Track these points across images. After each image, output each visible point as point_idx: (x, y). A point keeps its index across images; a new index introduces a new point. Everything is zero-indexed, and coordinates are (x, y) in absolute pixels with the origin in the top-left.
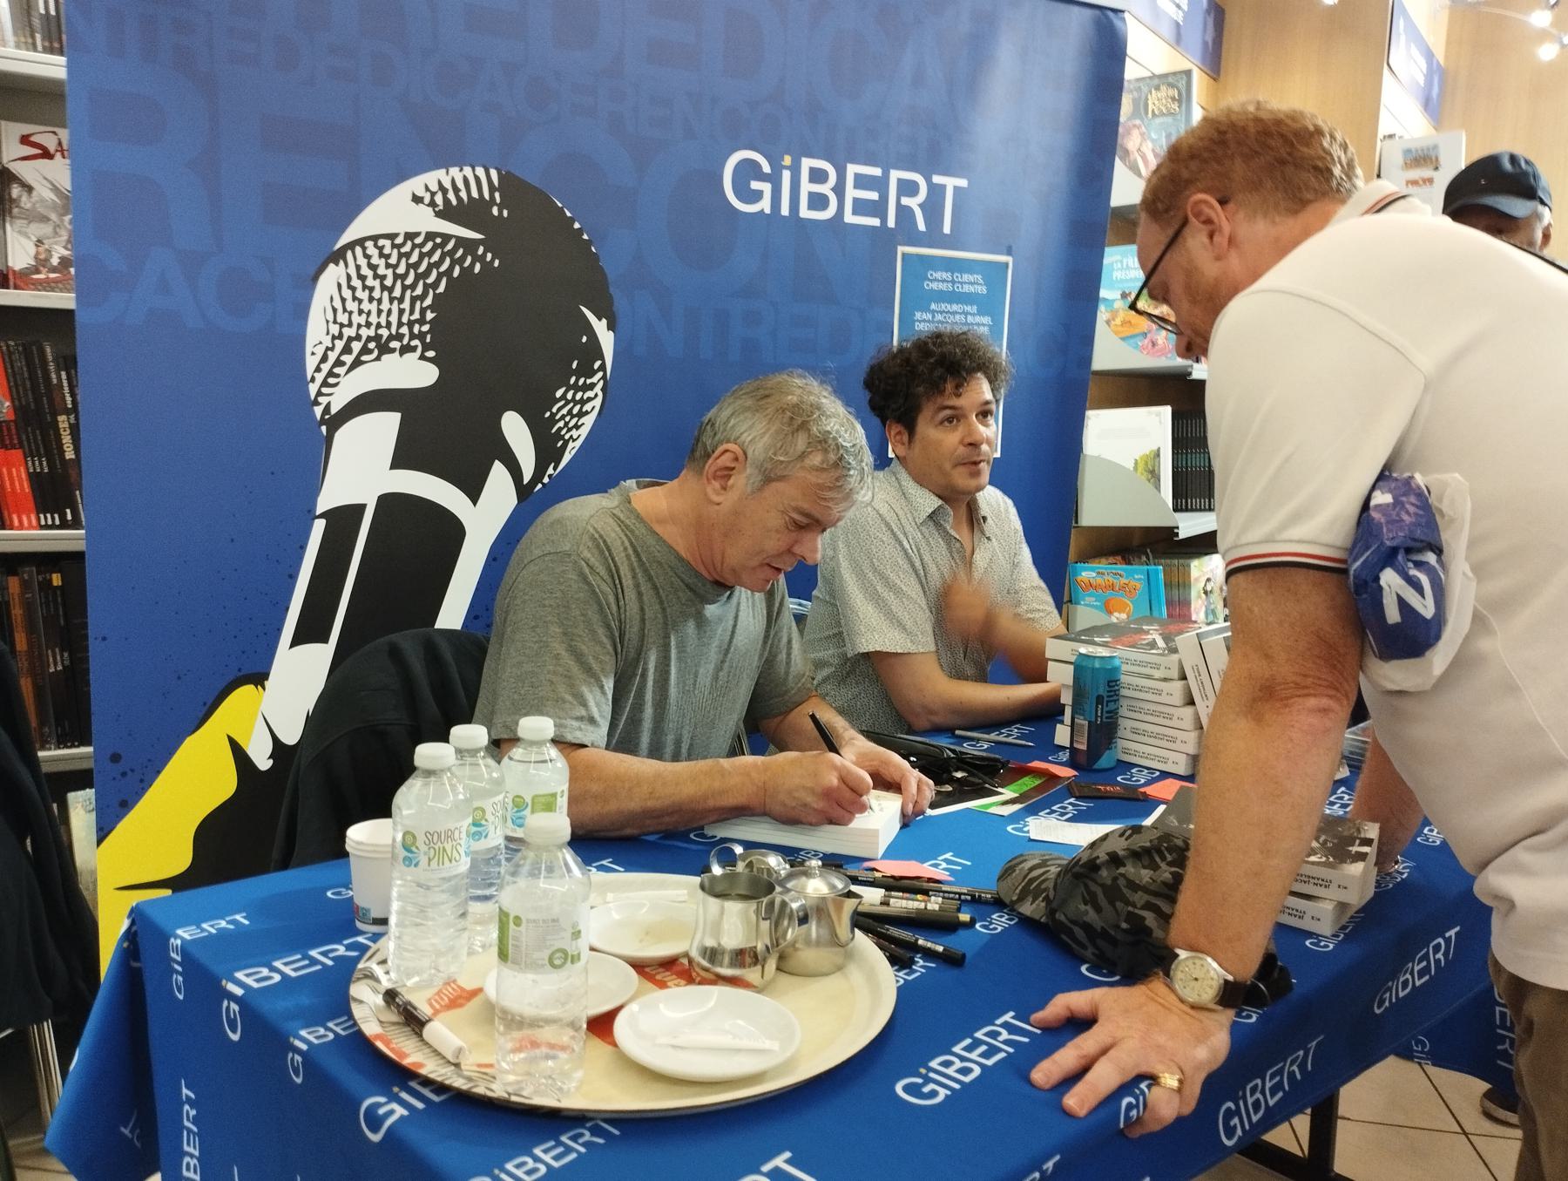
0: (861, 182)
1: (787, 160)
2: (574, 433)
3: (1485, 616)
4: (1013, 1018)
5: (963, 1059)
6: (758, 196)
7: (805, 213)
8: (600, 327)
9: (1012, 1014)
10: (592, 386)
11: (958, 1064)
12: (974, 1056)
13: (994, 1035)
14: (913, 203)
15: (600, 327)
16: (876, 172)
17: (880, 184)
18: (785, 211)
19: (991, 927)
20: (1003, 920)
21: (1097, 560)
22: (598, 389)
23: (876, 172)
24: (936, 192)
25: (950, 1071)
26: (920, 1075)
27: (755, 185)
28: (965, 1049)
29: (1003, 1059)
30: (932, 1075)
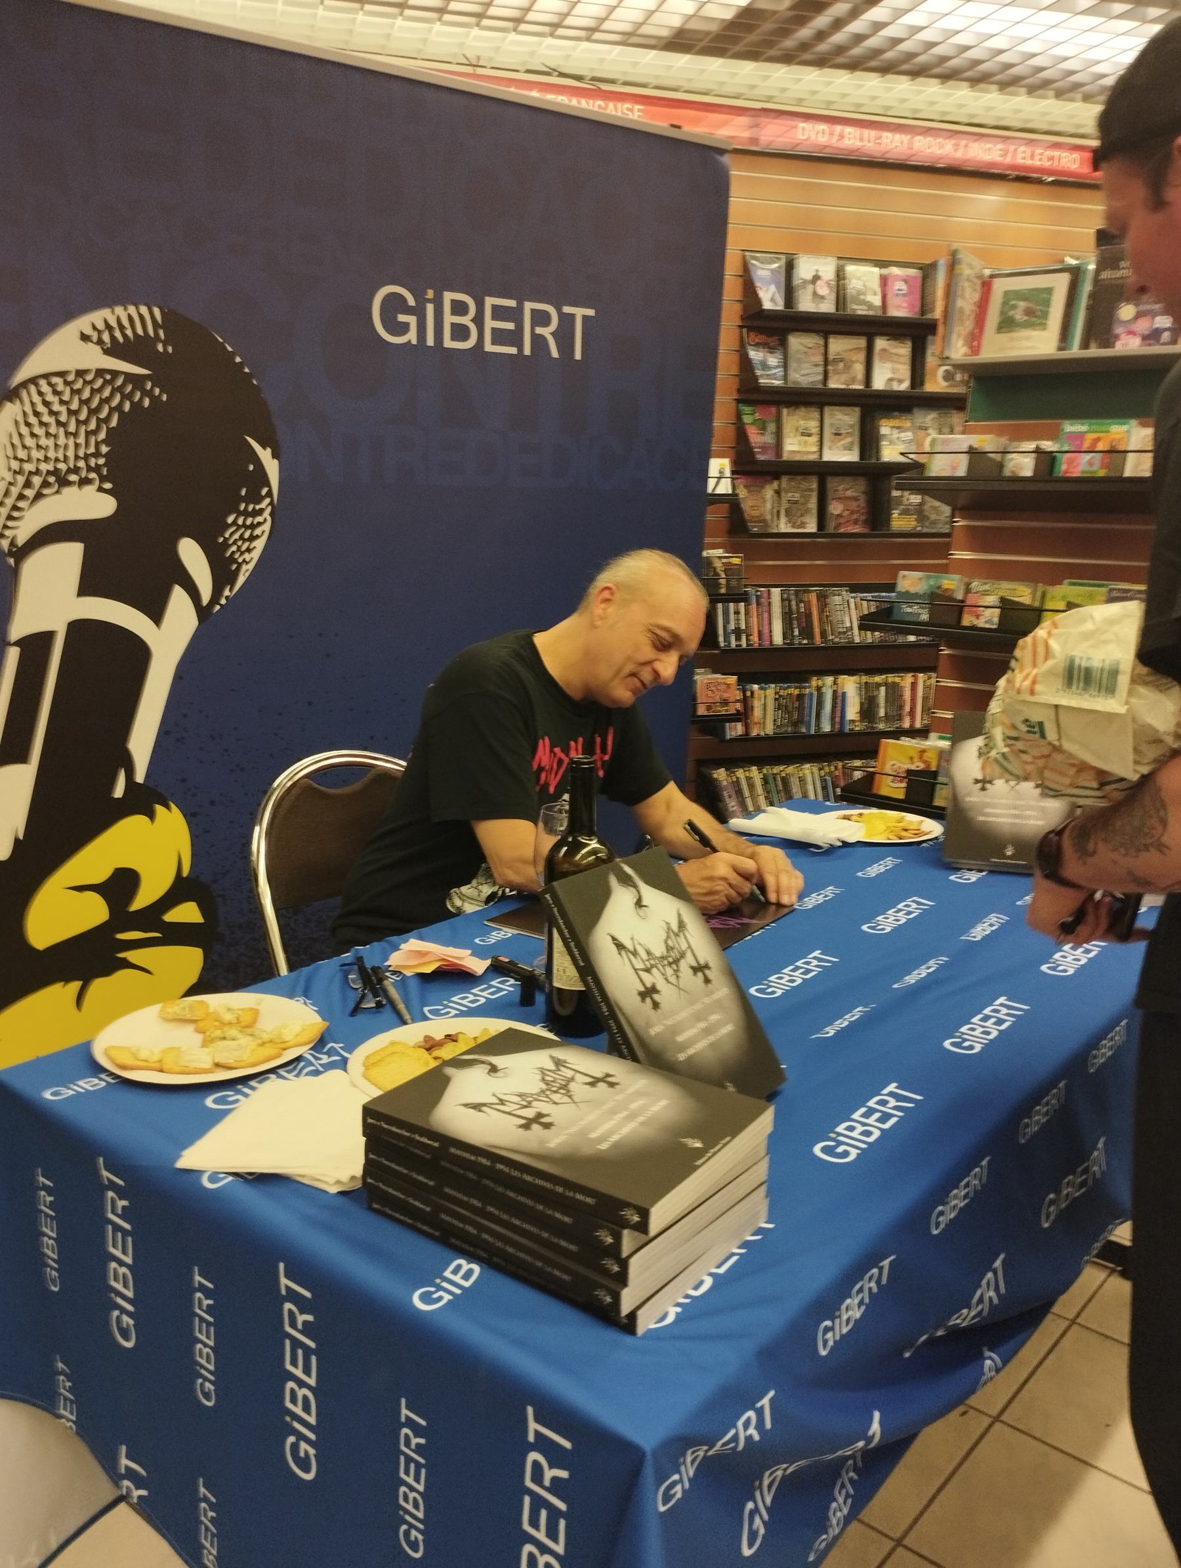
0: (498, 313)
1: (430, 294)
2: (247, 556)
6: (404, 328)
7: (448, 343)
8: (265, 455)
10: (261, 511)
13: (808, 963)
14: (546, 332)
15: (265, 455)
16: (512, 303)
17: (514, 315)
18: (430, 342)
22: (266, 514)
23: (512, 303)
24: (567, 321)
27: (402, 318)
28: (791, 971)
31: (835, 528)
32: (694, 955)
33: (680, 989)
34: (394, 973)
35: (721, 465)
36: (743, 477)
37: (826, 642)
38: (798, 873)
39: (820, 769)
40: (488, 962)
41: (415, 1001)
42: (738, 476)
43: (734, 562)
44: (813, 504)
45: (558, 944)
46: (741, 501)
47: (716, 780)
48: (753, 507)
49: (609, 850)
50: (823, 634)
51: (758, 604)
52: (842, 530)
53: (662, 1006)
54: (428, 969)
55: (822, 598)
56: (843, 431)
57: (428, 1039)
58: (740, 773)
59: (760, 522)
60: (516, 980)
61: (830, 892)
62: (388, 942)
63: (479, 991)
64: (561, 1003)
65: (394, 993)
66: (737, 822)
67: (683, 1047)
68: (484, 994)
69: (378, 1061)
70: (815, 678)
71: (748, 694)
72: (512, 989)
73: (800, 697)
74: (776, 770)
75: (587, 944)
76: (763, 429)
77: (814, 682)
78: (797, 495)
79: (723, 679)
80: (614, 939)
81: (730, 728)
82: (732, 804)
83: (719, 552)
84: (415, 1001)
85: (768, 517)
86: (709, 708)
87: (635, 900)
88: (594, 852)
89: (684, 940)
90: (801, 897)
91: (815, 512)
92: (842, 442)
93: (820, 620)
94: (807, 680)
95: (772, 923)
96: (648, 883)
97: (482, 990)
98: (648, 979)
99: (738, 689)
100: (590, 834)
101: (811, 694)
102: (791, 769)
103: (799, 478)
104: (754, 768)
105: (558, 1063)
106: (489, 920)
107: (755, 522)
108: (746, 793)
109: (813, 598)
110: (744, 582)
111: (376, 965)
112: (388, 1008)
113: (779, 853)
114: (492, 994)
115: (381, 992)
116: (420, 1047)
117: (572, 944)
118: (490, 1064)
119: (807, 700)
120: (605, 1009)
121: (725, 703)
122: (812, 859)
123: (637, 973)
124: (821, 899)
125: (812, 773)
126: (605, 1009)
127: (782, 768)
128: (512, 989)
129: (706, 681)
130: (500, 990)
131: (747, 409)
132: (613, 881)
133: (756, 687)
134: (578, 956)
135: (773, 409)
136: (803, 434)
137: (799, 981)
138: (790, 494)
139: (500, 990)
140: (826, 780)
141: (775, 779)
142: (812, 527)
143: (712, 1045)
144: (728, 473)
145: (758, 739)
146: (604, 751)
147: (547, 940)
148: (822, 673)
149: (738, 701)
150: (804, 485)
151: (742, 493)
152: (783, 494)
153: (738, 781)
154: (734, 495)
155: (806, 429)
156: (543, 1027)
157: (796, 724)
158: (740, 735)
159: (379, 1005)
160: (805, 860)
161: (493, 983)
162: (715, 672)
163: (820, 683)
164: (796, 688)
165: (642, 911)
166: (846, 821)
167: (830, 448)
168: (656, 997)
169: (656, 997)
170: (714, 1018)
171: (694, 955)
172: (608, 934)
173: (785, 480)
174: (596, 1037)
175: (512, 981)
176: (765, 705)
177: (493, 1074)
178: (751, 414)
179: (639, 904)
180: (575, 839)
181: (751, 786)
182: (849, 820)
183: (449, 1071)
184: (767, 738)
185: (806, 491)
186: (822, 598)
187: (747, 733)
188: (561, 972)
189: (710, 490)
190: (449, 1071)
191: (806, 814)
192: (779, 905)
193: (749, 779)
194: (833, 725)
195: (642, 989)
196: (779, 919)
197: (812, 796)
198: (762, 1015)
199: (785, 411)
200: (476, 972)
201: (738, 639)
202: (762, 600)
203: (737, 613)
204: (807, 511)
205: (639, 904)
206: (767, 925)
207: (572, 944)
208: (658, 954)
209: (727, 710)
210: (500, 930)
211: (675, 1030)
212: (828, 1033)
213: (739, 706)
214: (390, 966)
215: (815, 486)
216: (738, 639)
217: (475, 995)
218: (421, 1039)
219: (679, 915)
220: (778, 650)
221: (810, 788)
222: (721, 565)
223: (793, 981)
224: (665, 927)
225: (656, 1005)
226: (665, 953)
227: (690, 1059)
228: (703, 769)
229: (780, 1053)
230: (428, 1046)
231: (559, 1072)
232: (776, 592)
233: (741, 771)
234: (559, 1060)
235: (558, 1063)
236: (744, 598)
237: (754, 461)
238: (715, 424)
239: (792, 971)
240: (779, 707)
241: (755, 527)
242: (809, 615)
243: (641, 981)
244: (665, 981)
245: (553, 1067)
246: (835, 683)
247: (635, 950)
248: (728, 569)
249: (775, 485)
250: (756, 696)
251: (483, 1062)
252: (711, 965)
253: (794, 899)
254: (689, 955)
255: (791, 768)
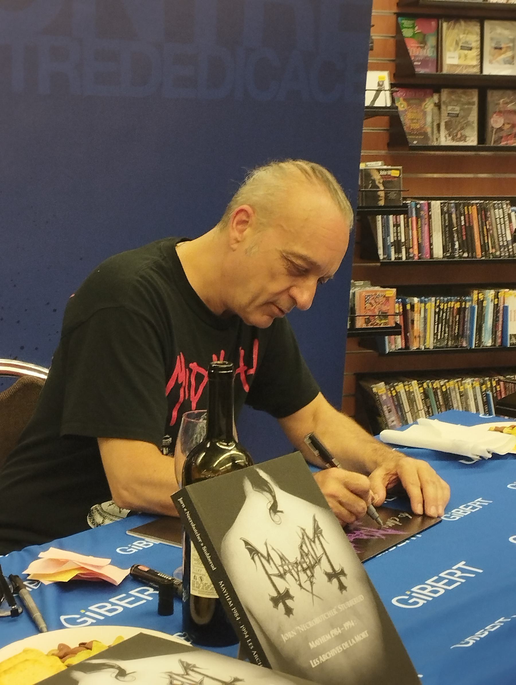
3: (231, 455)
4: (464, 565)
5: (432, 586)
9: (464, 563)
11: (430, 589)
12: (440, 584)
13: (452, 574)
19: (411, 601)
20: (425, 592)
21: (306, 162)
25: (425, 592)
26: (407, 595)
28: (434, 581)
29: (459, 585)
30: (413, 594)
31: (495, 142)
32: (329, 561)
33: (313, 595)
34: (32, 582)
35: (380, 78)
36: (401, 89)
37: (486, 256)
38: (444, 483)
39: (481, 385)
40: (127, 572)
41: (51, 610)
42: (397, 89)
43: (393, 175)
44: (474, 117)
45: (194, 553)
46: (400, 114)
47: (376, 394)
48: (413, 119)
49: (247, 456)
50: (484, 247)
51: (418, 217)
52: (503, 144)
53: (294, 612)
54: (66, 578)
55: (483, 211)
56: (503, 46)
57: (62, 647)
58: (400, 387)
59: (421, 134)
60: (155, 589)
61: (478, 503)
62: (27, 551)
63: (118, 600)
64: (198, 612)
65: (31, 603)
66: (386, 434)
67: (316, 654)
68: (123, 603)
69: (10, 669)
70: (476, 292)
71: (408, 307)
72: (150, 598)
73: (461, 311)
74: (437, 384)
75: (220, 549)
76: (423, 42)
77: (475, 295)
78: (457, 108)
79: (382, 291)
80: (247, 543)
81: (389, 342)
82: (392, 418)
83: (378, 165)
84: (51, 610)
85: (429, 130)
86: (367, 321)
87: (270, 505)
88: (232, 459)
89: (319, 546)
90: (448, 509)
91: (475, 125)
92: (503, 56)
93: (481, 232)
94: (468, 294)
95: (418, 534)
96: (283, 487)
97: (121, 600)
98: (282, 585)
99: (398, 302)
100: (229, 439)
101: (472, 308)
102: (452, 383)
103: (460, 91)
104: (414, 383)
105: (187, 668)
106: (131, 531)
107: (416, 135)
108: (406, 407)
109: (474, 211)
110: (403, 194)
111: (14, 574)
112: (24, 617)
113: (423, 465)
114: (130, 603)
115: (17, 601)
116: (53, 655)
117: (204, 549)
118: (119, 668)
119: (467, 313)
120: (236, 614)
121: (384, 315)
122: (464, 470)
123: (270, 579)
124: (468, 511)
125: (474, 388)
126: (236, 614)
127: (442, 383)
128: (150, 598)
129: (364, 294)
130: (138, 599)
131: (406, 23)
132: (248, 485)
133: (416, 300)
134: (210, 560)
135: (433, 23)
136: (462, 48)
137: (442, 592)
138: (450, 108)
139: (138, 599)
140: (487, 396)
141: (436, 394)
142: (472, 140)
143: (344, 652)
144: (387, 86)
145: (418, 352)
146: (249, 364)
147: (184, 550)
148: (483, 286)
149: (396, 314)
150: (464, 99)
151: (402, 106)
152: (443, 107)
153: (398, 396)
154: (393, 107)
155: (467, 42)
156: (180, 636)
157: (456, 338)
158: (399, 349)
159: (15, 614)
160: (455, 472)
161: (132, 592)
162: (374, 284)
163: (481, 297)
164: (457, 301)
165: (276, 517)
166: (499, 433)
167: (491, 62)
168: (289, 602)
169: (289, 602)
170: (348, 625)
171: (329, 561)
172: (241, 539)
173: (445, 93)
174: (232, 646)
175: (151, 591)
176: (425, 318)
177: (121, 678)
178: (412, 28)
179: (274, 508)
180: (213, 445)
181: (412, 401)
182: (502, 432)
183: (77, 675)
184: (427, 352)
185: (466, 104)
186: (483, 211)
187: (407, 347)
188: (198, 580)
189: (367, 103)
190: (77, 675)
191: (459, 426)
192: (425, 516)
193: (409, 394)
194: (494, 340)
195: (275, 594)
196: (426, 530)
197: (473, 410)
198: (399, 626)
199: (445, 25)
200: (116, 582)
201: (398, 251)
202: (422, 213)
203: (397, 225)
204: (468, 124)
205: (274, 508)
206: (413, 536)
207: (204, 549)
208: (292, 560)
209: (385, 323)
210: (143, 540)
211: (307, 637)
212: (468, 643)
213: (399, 319)
214: (29, 575)
215: (475, 99)
216: (398, 251)
217: (113, 604)
218: (56, 648)
219: (315, 520)
220: (439, 263)
221: (472, 403)
222: (379, 177)
223: (436, 592)
224: (300, 533)
225: (289, 611)
226: (299, 559)
227: (322, 666)
228: (363, 384)
229: (416, 662)
230: (62, 654)
231: (187, 677)
232: (436, 205)
233: (401, 385)
234: (188, 665)
235: (187, 668)
236: (404, 210)
237: (413, 74)
238: (373, 38)
239: (436, 581)
240: (439, 321)
241: (415, 139)
242: (469, 229)
243: (274, 586)
244: (299, 587)
245: (181, 671)
246: (497, 296)
247: (269, 555)
248: (388, 182)
249: (436, 98)
250: (416, 309)
251: (112, 667)
252: (346, 572)
253: (441, 511)
254: (324, 560)
255: (451, 382)
